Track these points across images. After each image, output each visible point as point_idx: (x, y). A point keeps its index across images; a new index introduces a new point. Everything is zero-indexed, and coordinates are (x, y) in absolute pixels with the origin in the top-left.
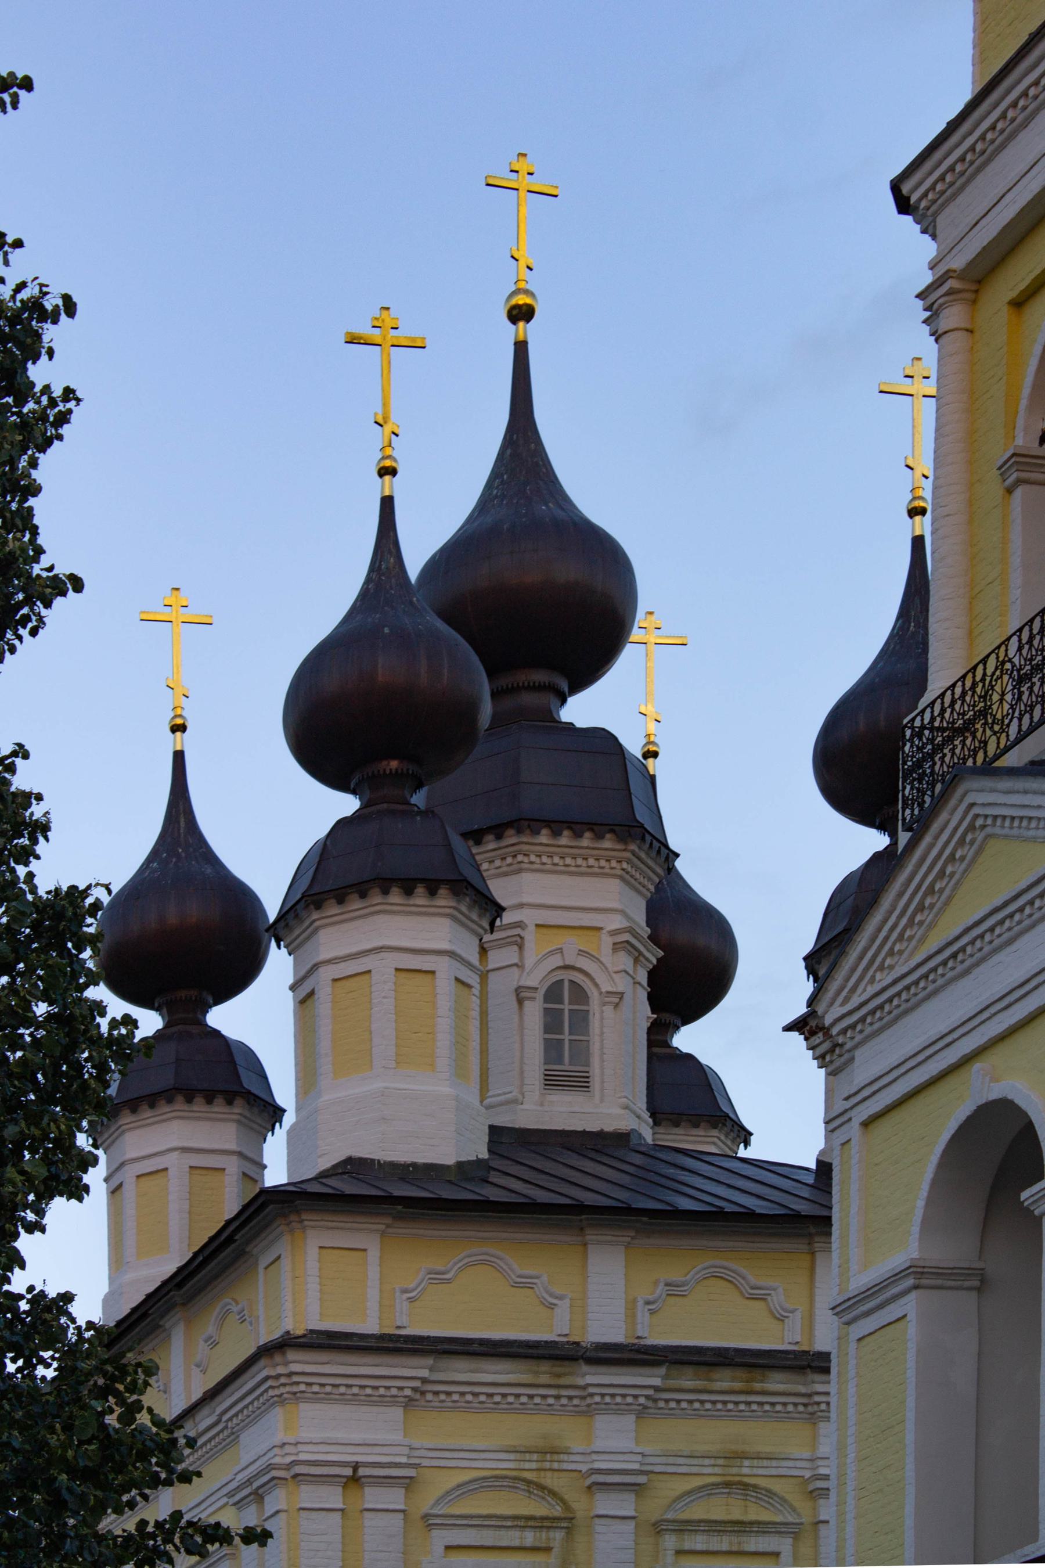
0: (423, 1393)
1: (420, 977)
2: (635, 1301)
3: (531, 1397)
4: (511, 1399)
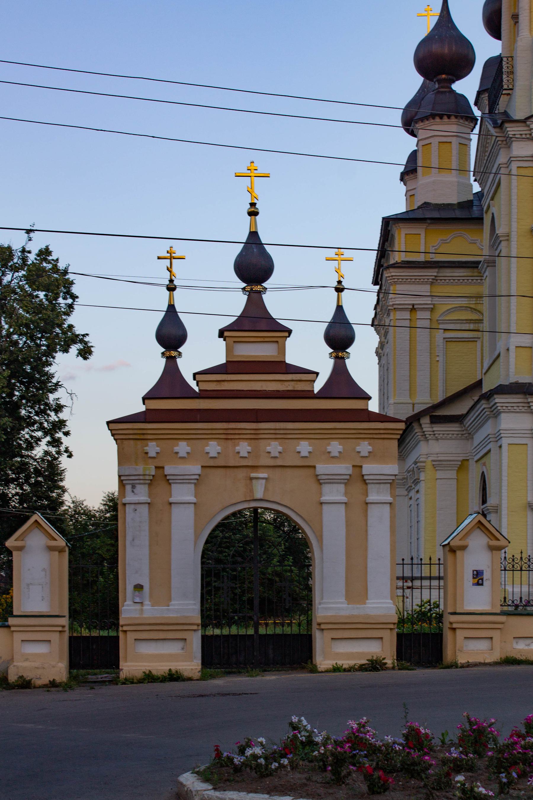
0: (437, 280)
1: (446, 145)
3: (472, 280)
4: (466, 281)
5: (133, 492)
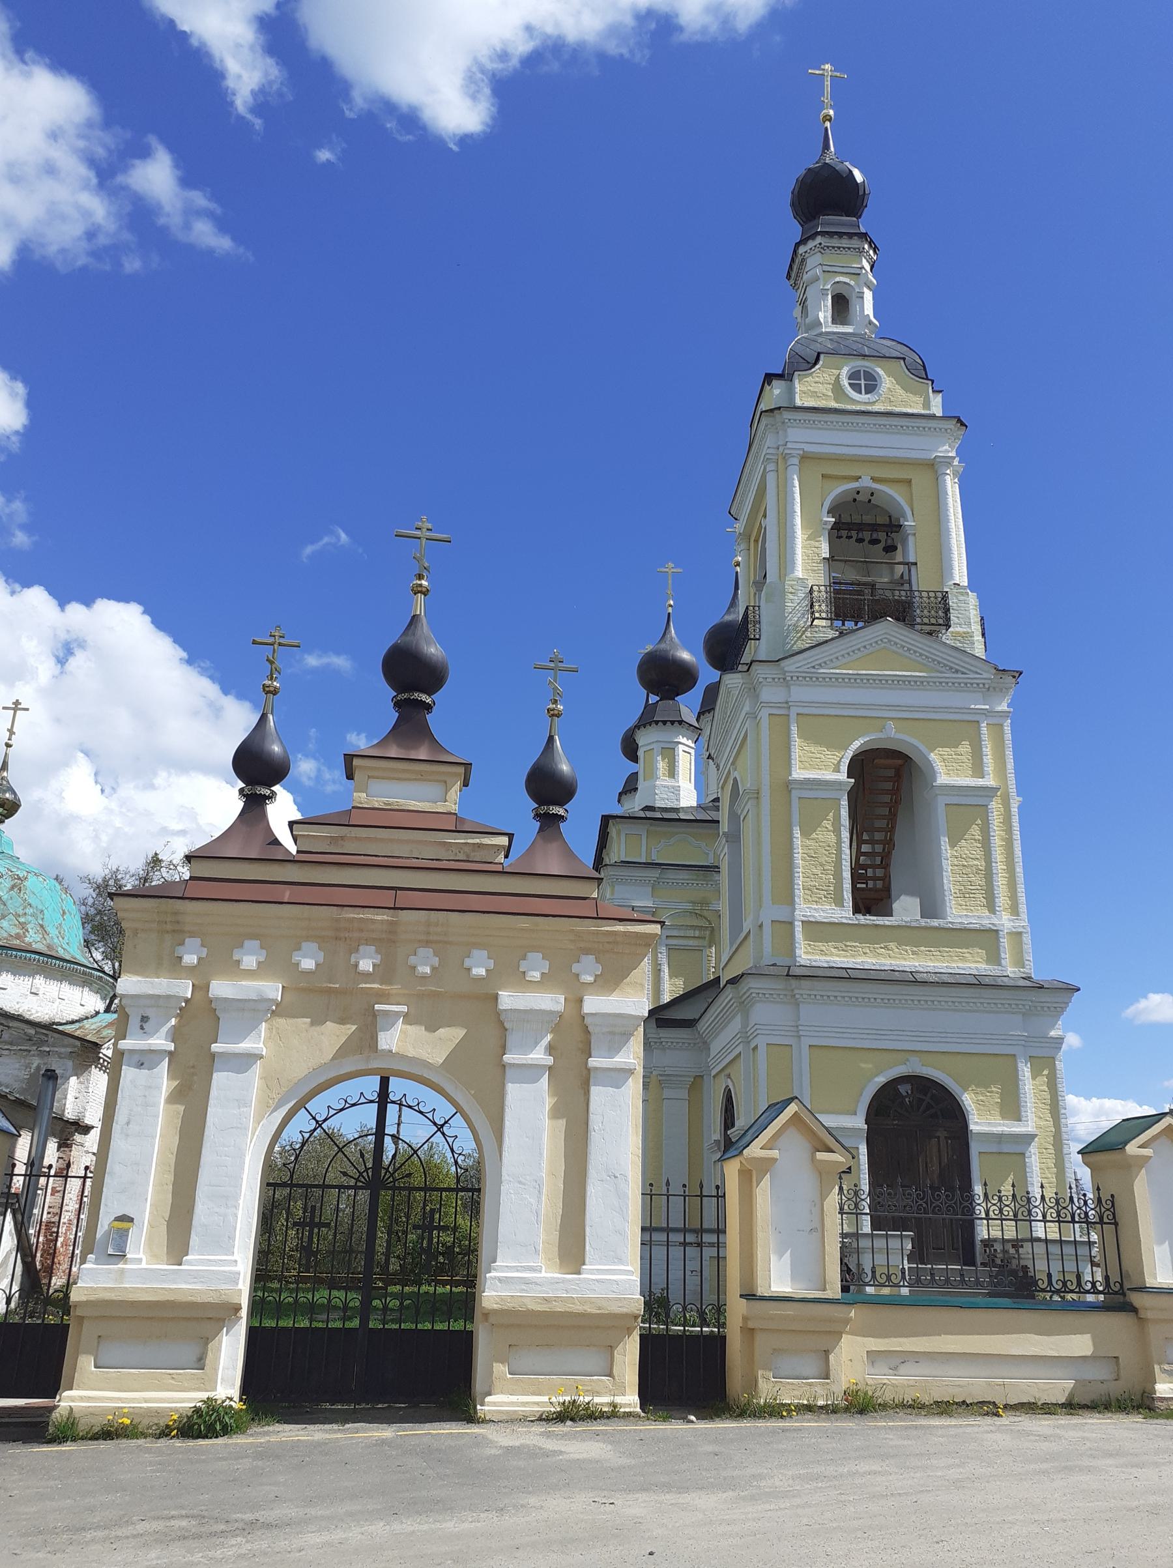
5: (142, 1028)
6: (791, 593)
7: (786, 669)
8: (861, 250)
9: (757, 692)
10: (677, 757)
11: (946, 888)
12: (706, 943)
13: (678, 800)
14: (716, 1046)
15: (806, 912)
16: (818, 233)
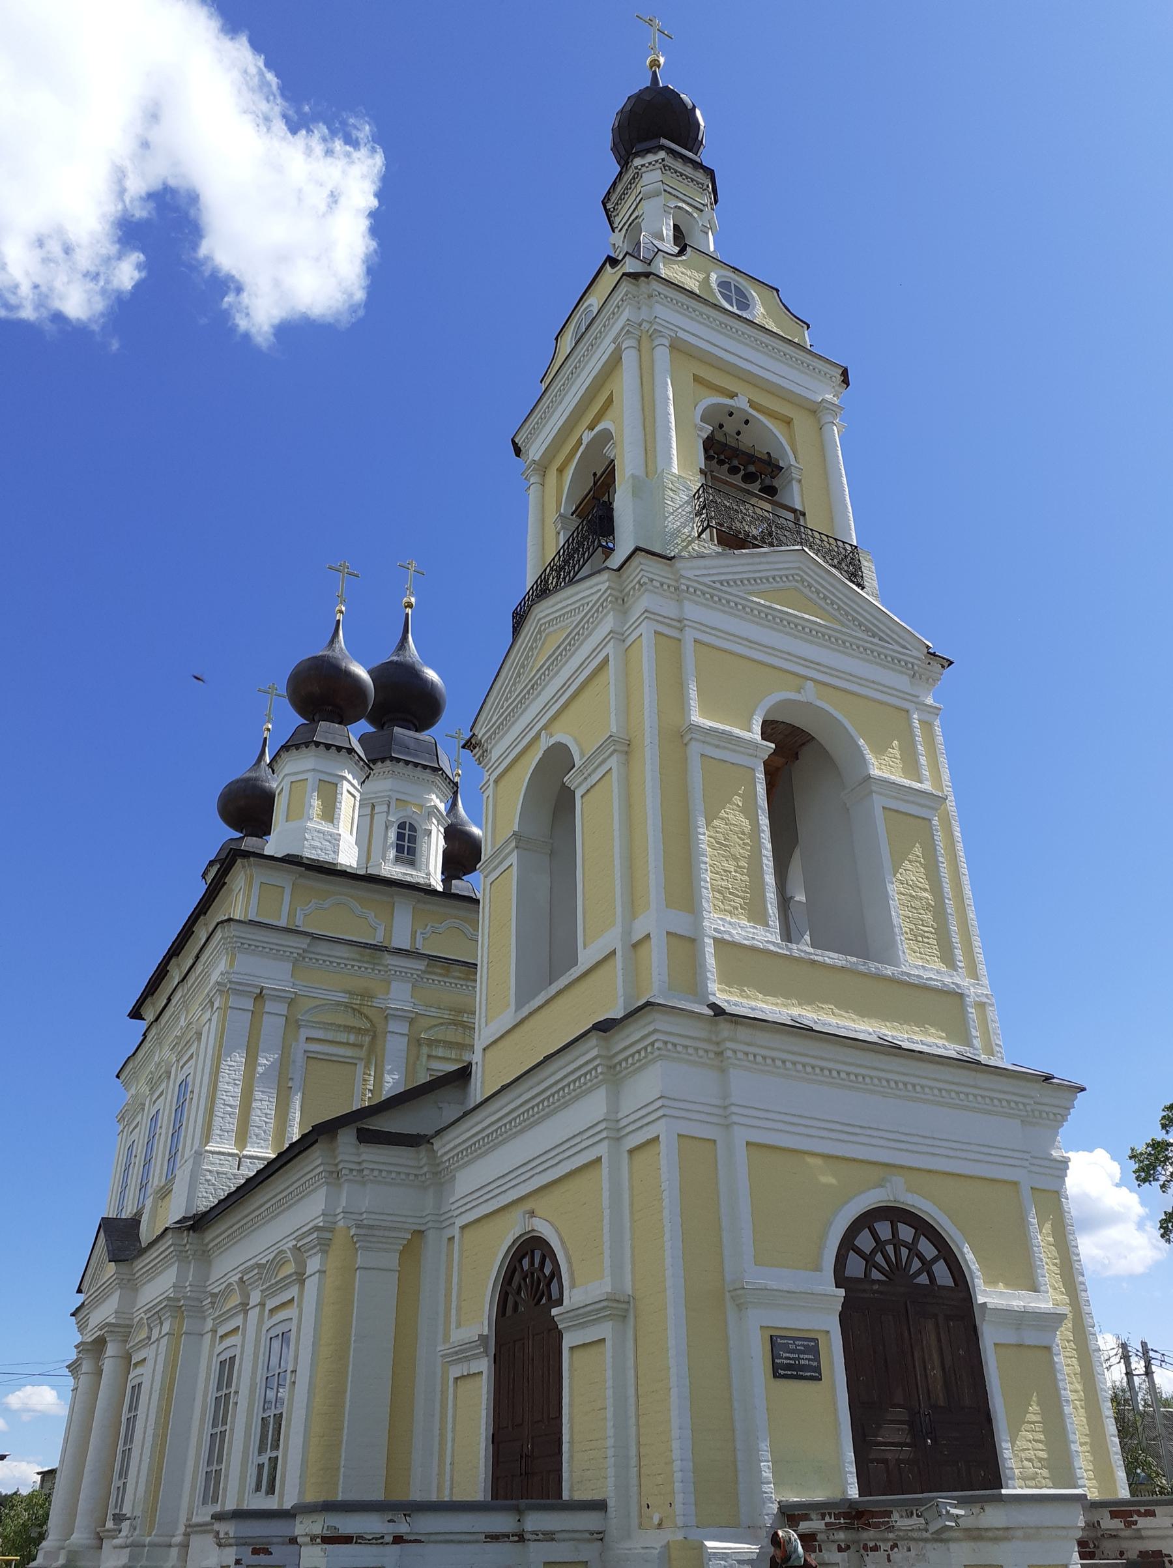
2: (416, 932)
6: (671, 490)
7: (683, 572)
8: (705, 187)
9: (627, 605)
10: (339, 796)
11: (895, 922)
12: (363, 1053)
13: (336, 852)
14: (468, 1180)
15: (718, 924)
16: (662, 147)
